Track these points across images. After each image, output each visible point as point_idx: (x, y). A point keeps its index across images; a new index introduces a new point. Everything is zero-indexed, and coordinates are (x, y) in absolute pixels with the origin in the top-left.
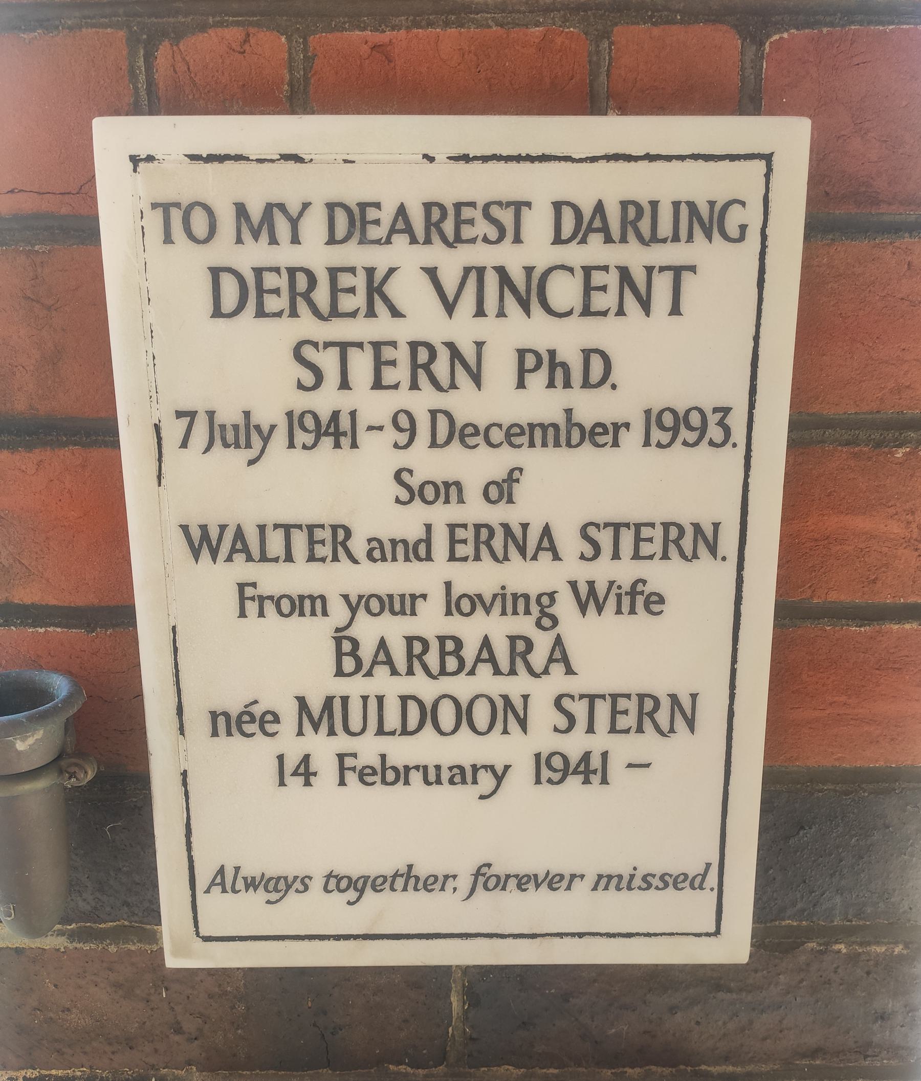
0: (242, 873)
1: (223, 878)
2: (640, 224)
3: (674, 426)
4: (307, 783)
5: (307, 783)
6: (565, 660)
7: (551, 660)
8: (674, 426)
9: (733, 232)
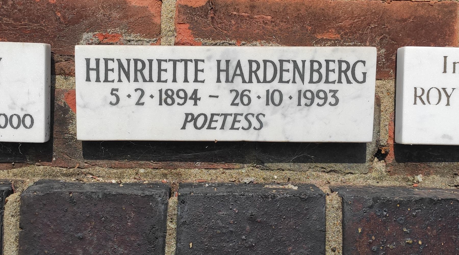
9: (360, 77)
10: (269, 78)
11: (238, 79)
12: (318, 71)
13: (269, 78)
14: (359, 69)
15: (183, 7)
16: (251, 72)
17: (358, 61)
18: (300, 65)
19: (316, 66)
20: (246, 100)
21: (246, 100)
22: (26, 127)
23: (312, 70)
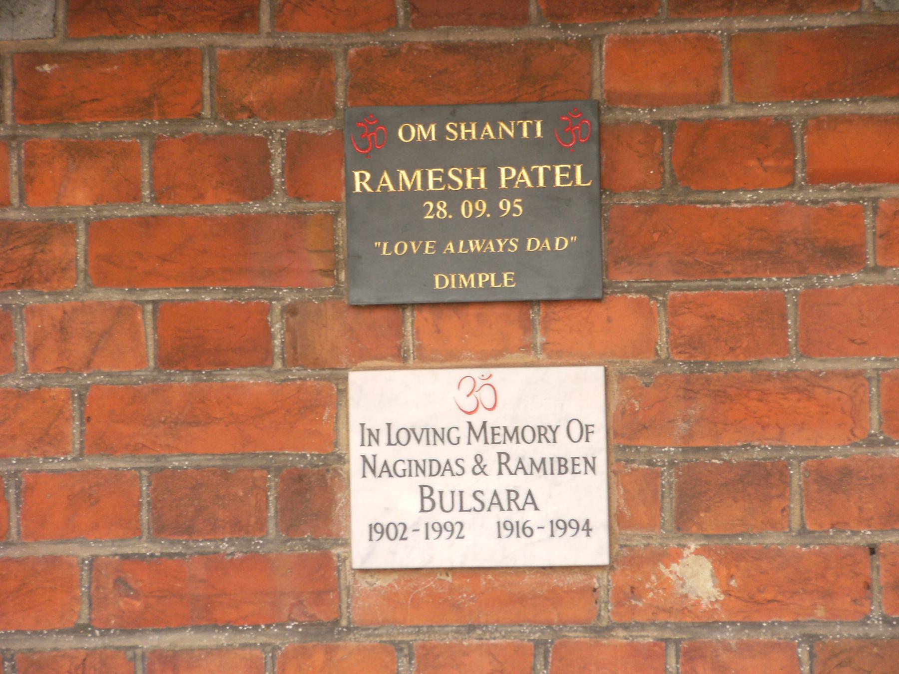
0: (366, 427)
1: (387, 467)
2: (517, 501)
3: (560, 526)
4: (588, 535)
5: (588, 535)
6: (534, 503)
7: (518, 468)
8: (560, 526)
9: (454, 440)
10: (434, 472)
11: (495, 509)
12: (565, 466)
13: (434, 472)
14: (454, 435)
15: (678, 529)
16: (509, 500)
17: (570, 422)
18: (421, 464)
19: (563, 462)
20: (528, 532)
21: (528, 532)
22: (439, 523)
23: (560, 466)
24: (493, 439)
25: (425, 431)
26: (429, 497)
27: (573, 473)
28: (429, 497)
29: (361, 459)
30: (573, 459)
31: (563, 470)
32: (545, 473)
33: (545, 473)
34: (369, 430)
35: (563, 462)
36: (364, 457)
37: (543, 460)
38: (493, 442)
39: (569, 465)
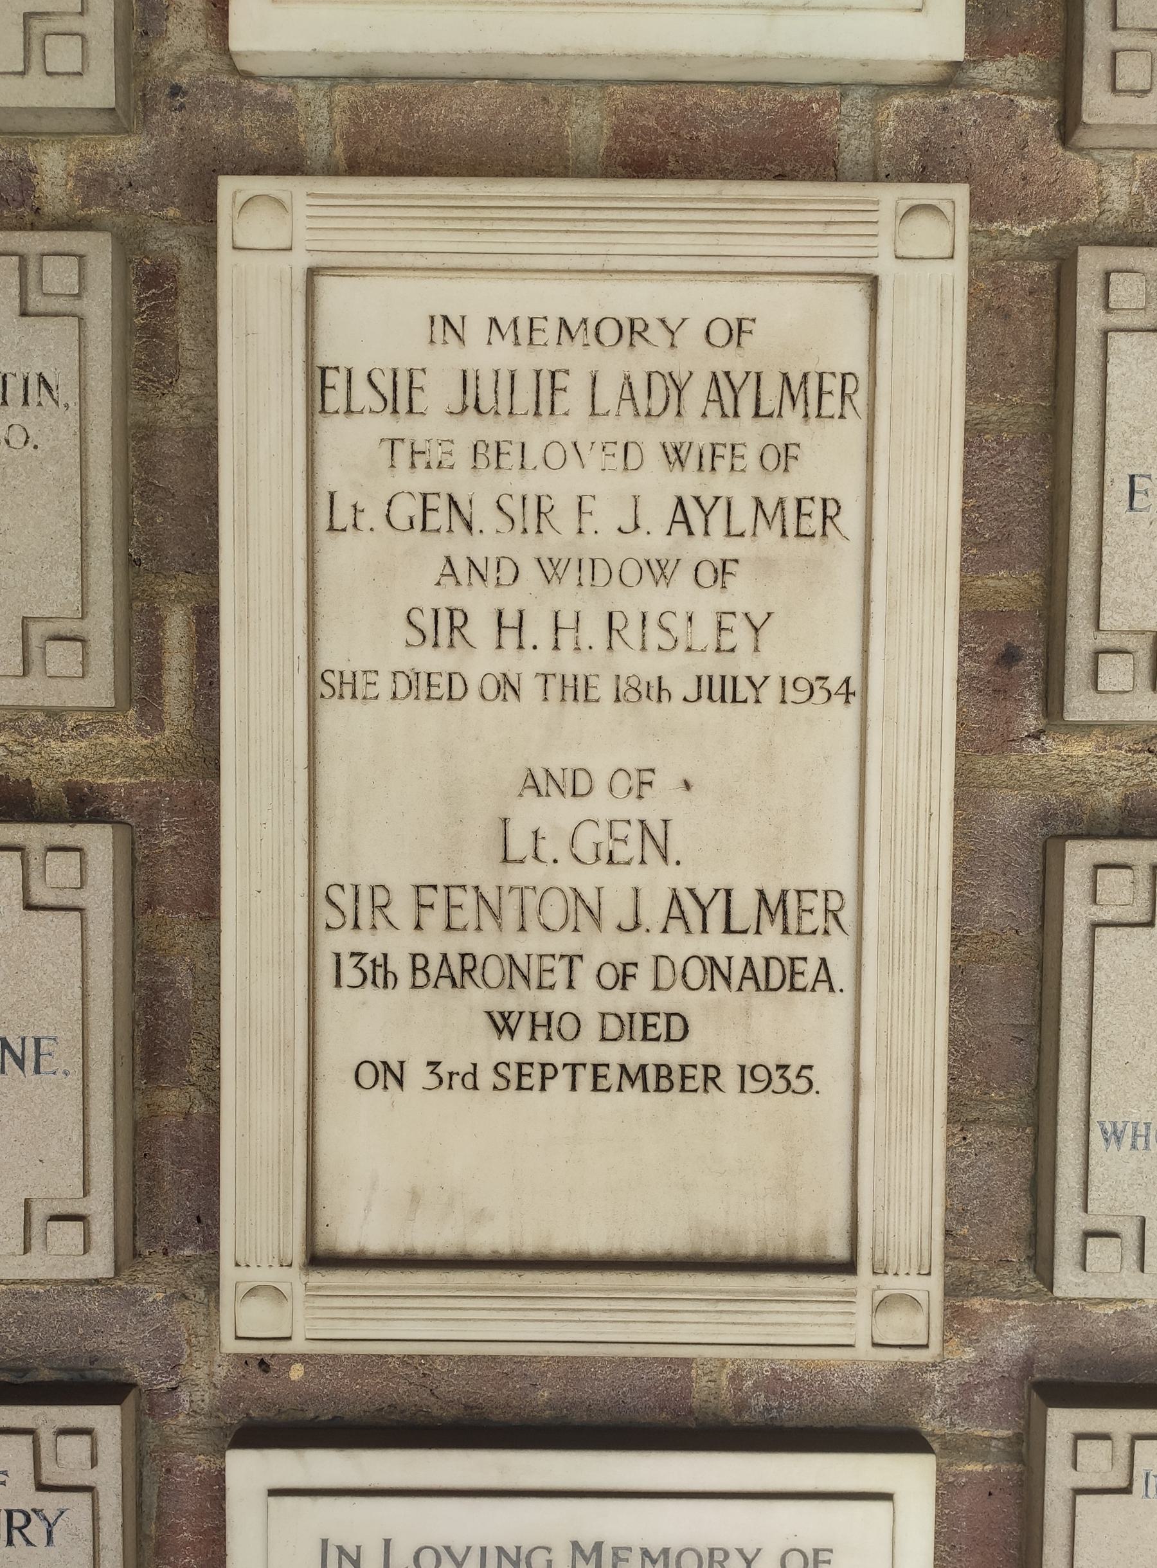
23: (659, 1077)
24: (645, 1033)
25: (722, 895)
26: (423, 969)
27: (683, 1089)
28: (423, 969)
29: (757, 896)
30: (683, 1068)
31: (665, 1084)
32: (645, 1089)
33: (645, 1089)
34: (1101, 1124)
35: (664, 1071)
36: (761, 892)
37: (643, 1068)
38: (645, 1038)
39: (676, 1077)
